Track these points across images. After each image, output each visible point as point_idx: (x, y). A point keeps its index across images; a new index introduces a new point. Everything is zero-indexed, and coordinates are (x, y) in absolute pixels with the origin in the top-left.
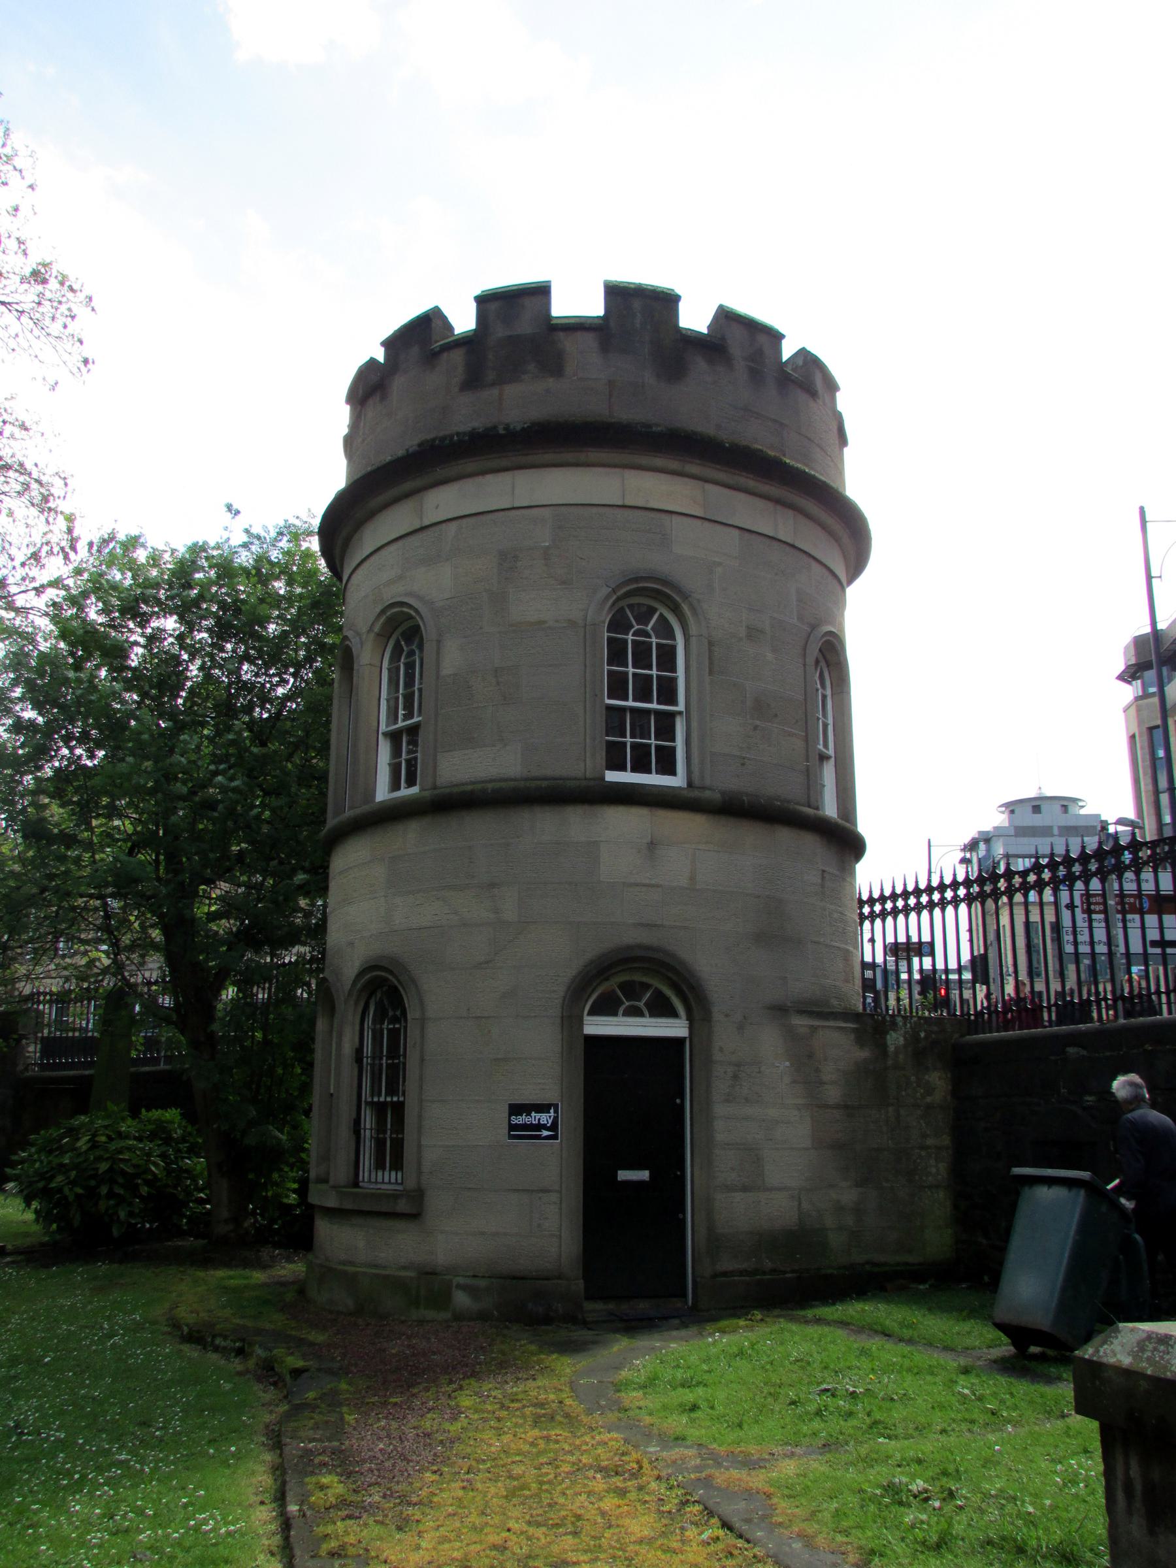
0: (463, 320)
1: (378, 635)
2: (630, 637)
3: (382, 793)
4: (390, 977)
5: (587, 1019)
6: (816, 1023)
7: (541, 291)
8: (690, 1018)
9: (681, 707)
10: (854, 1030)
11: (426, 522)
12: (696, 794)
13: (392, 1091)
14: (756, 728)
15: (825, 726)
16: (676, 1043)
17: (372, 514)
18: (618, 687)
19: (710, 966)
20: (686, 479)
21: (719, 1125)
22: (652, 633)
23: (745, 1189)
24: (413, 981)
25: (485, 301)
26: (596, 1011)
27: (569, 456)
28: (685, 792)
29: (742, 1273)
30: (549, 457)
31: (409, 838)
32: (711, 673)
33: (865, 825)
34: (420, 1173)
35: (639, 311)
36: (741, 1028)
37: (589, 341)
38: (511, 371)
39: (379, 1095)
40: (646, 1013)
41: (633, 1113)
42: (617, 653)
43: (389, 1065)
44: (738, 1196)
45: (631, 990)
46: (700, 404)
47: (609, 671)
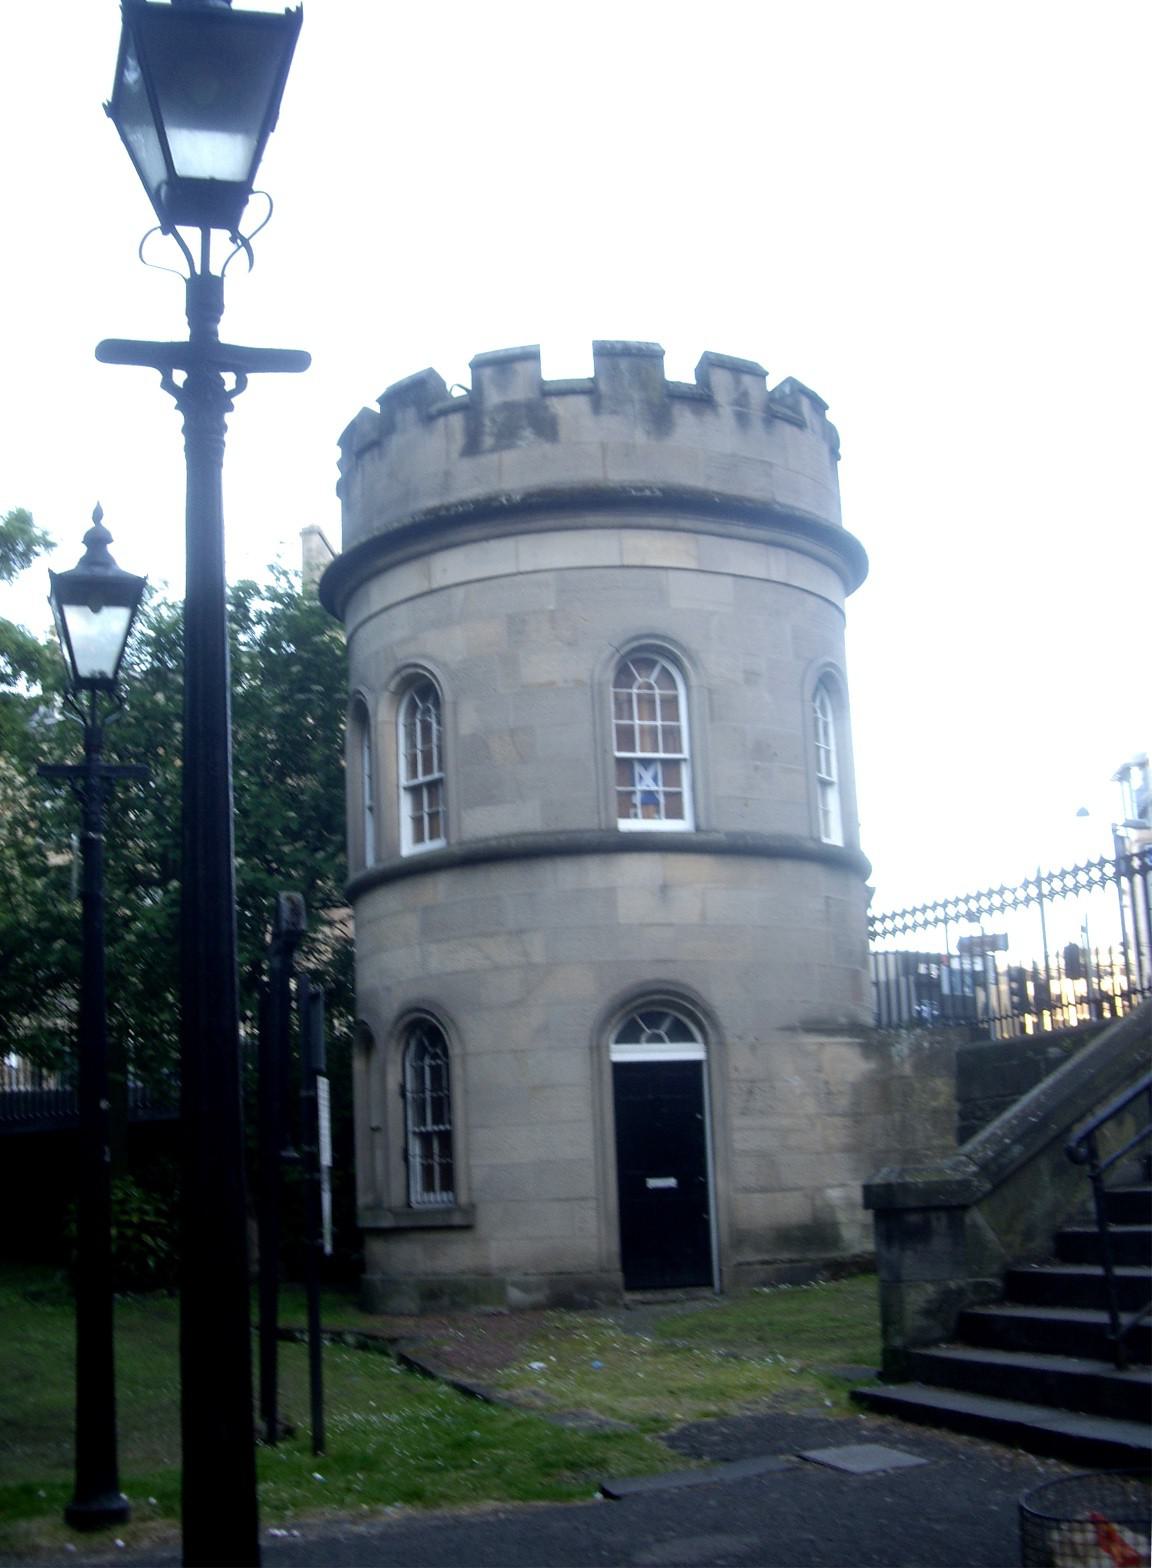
0: (457, 381)
1: (393, 693)
2: (635, 691)
3: (408, 848)
4: (428, 1017)
5: (614, 1047)
6: (823, 1039)
7: (531, 356)
8: (706, 1042)
9: (685, 754)
10: (860, 1045)
11: (435, 585)
12: (702, 837)
13: (437, 1120)
14: (756, 768)
15: (828, 752)
16: (694, 1067)
17: (379, 572)
18: (626, 738)
19: (720, 996)
20: (682, 534)
21: (737, 1136)
22: (655, 685)
23: (764, 1190)
24: (452, 1020)
25: (478, 365)
26: (620, 1040)
27: (567, 522)
28: (694, 838)
29: (764, 1263)
30: (551, 523)
31: (439, 889)
32: (712, 719)
33: (869, 846)
34: (470, 1189)
35: (628, 365)
36: (753, 1048)
37: (582, 403)
38: (507, 436)
39: (425, 1125)
40: (666, 1038)
41: (660, 1124)
42: (623, 706)
43: (435, 1099)
44: (757, 1196)
45: (653, 1018)
46: (696, 454)
47: (618, 726)
